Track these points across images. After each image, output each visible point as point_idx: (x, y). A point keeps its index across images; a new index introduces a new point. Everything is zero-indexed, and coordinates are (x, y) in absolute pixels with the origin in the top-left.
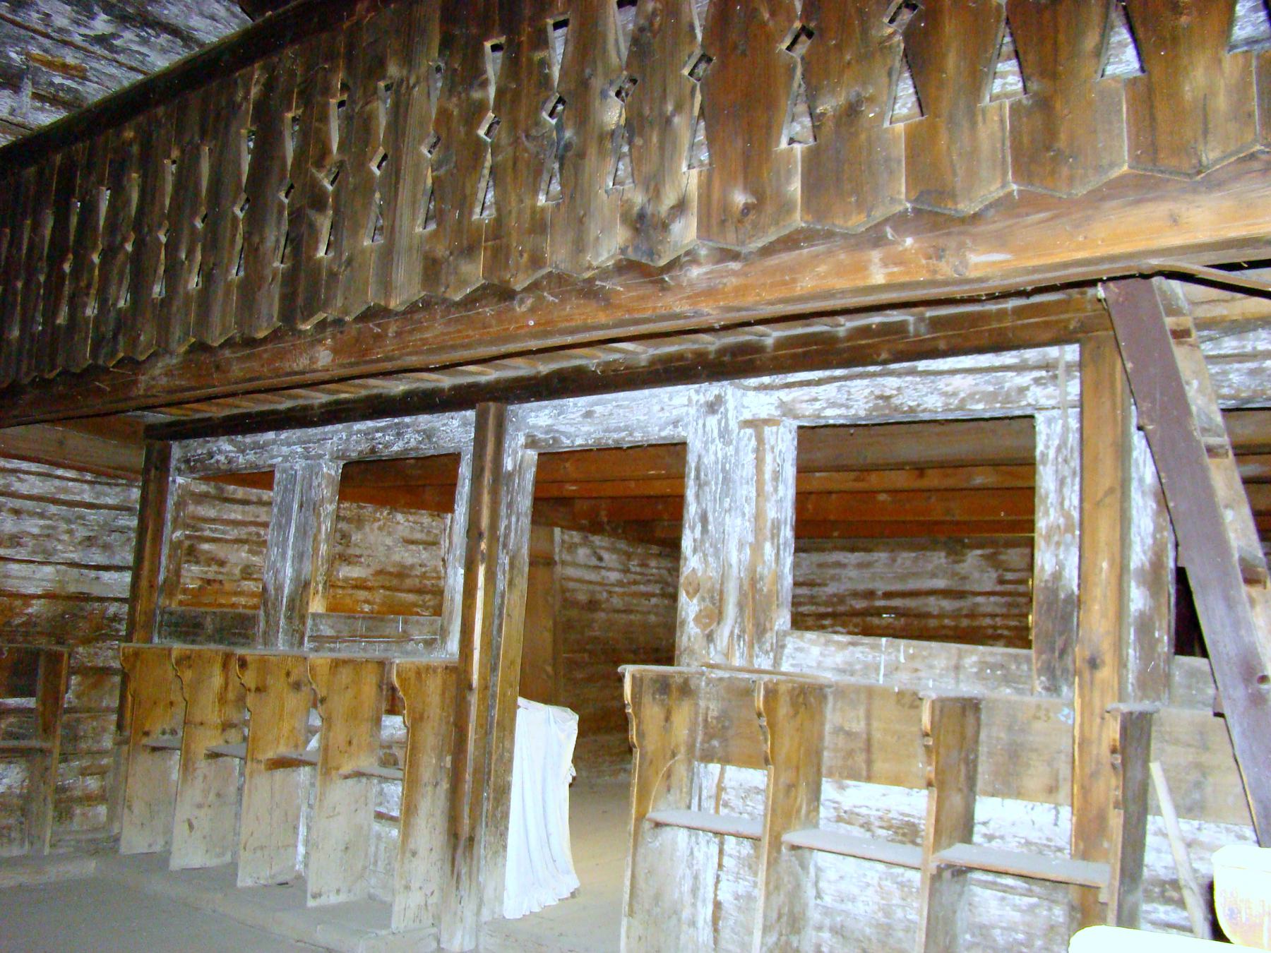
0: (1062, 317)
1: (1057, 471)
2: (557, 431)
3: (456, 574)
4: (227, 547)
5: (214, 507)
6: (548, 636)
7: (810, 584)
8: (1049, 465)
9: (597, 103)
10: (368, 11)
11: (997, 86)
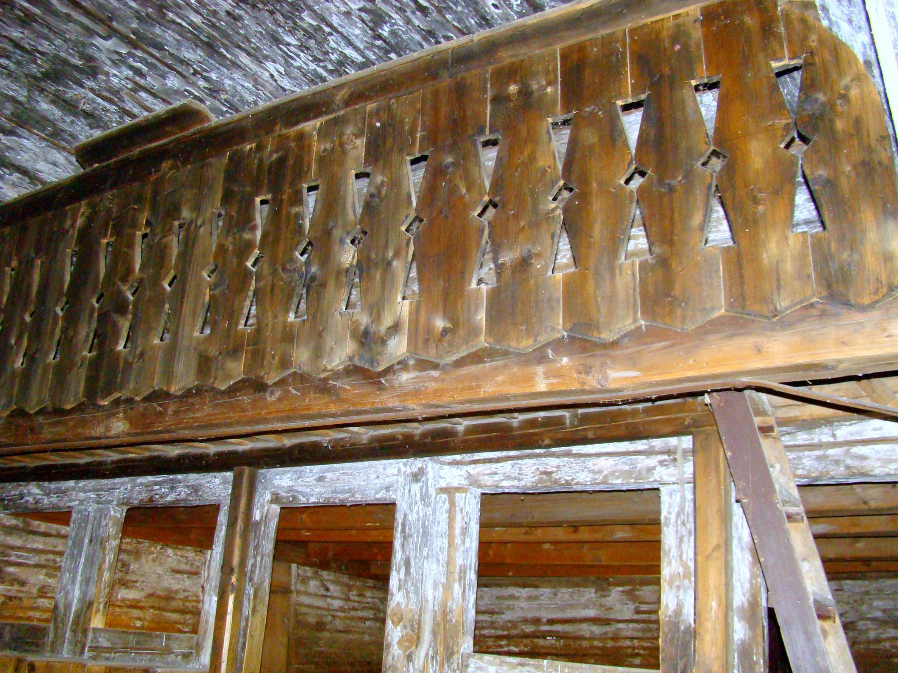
0: (680, 415)
1: (677, 531)
2: (297, 491)
3: (211, 601)
4: (27, 570)
5: (21, 537)
6: (283, 651)
7: (492, 613)
8: (671, 526)
9: (337, 247)
10: (171, 169)
11: (631, 246)
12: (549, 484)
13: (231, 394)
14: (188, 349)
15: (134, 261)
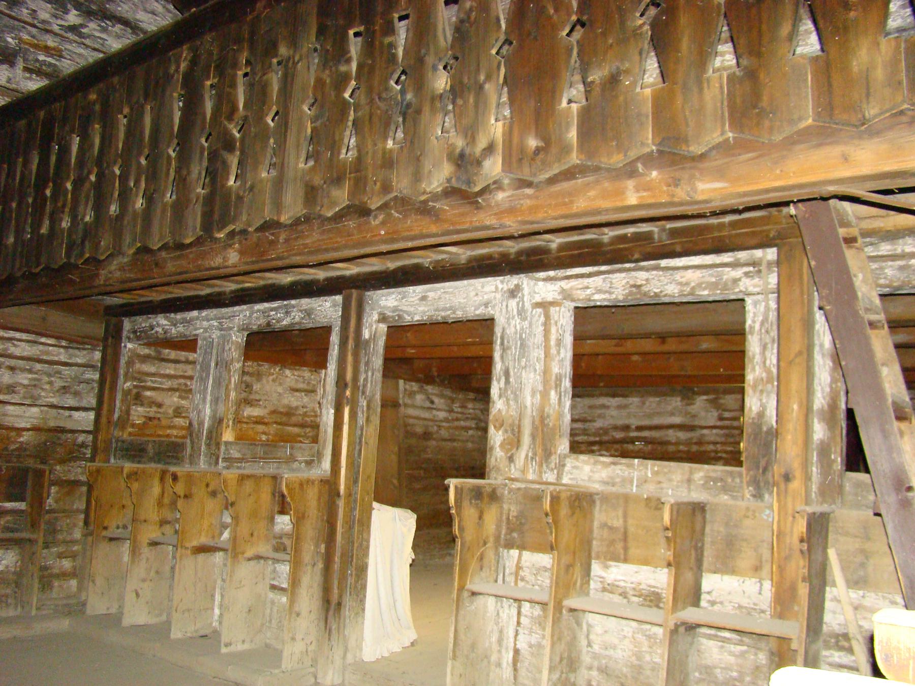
0: (765, 228)
1: (761, 339)
2: (401, 310)
3: (328, 413)
4: (164, 394)
6: (394, 458)
7: (584, 421)
9: (430, 74)
10: (265, 8)
11: (718, 62)
12: (639, 296)
13: (338, 221)
14: (295, 179)
15: (238, 100)
